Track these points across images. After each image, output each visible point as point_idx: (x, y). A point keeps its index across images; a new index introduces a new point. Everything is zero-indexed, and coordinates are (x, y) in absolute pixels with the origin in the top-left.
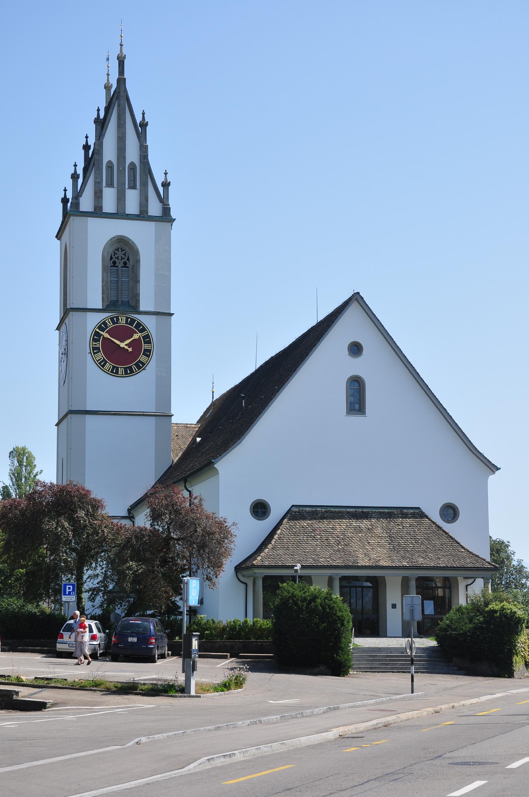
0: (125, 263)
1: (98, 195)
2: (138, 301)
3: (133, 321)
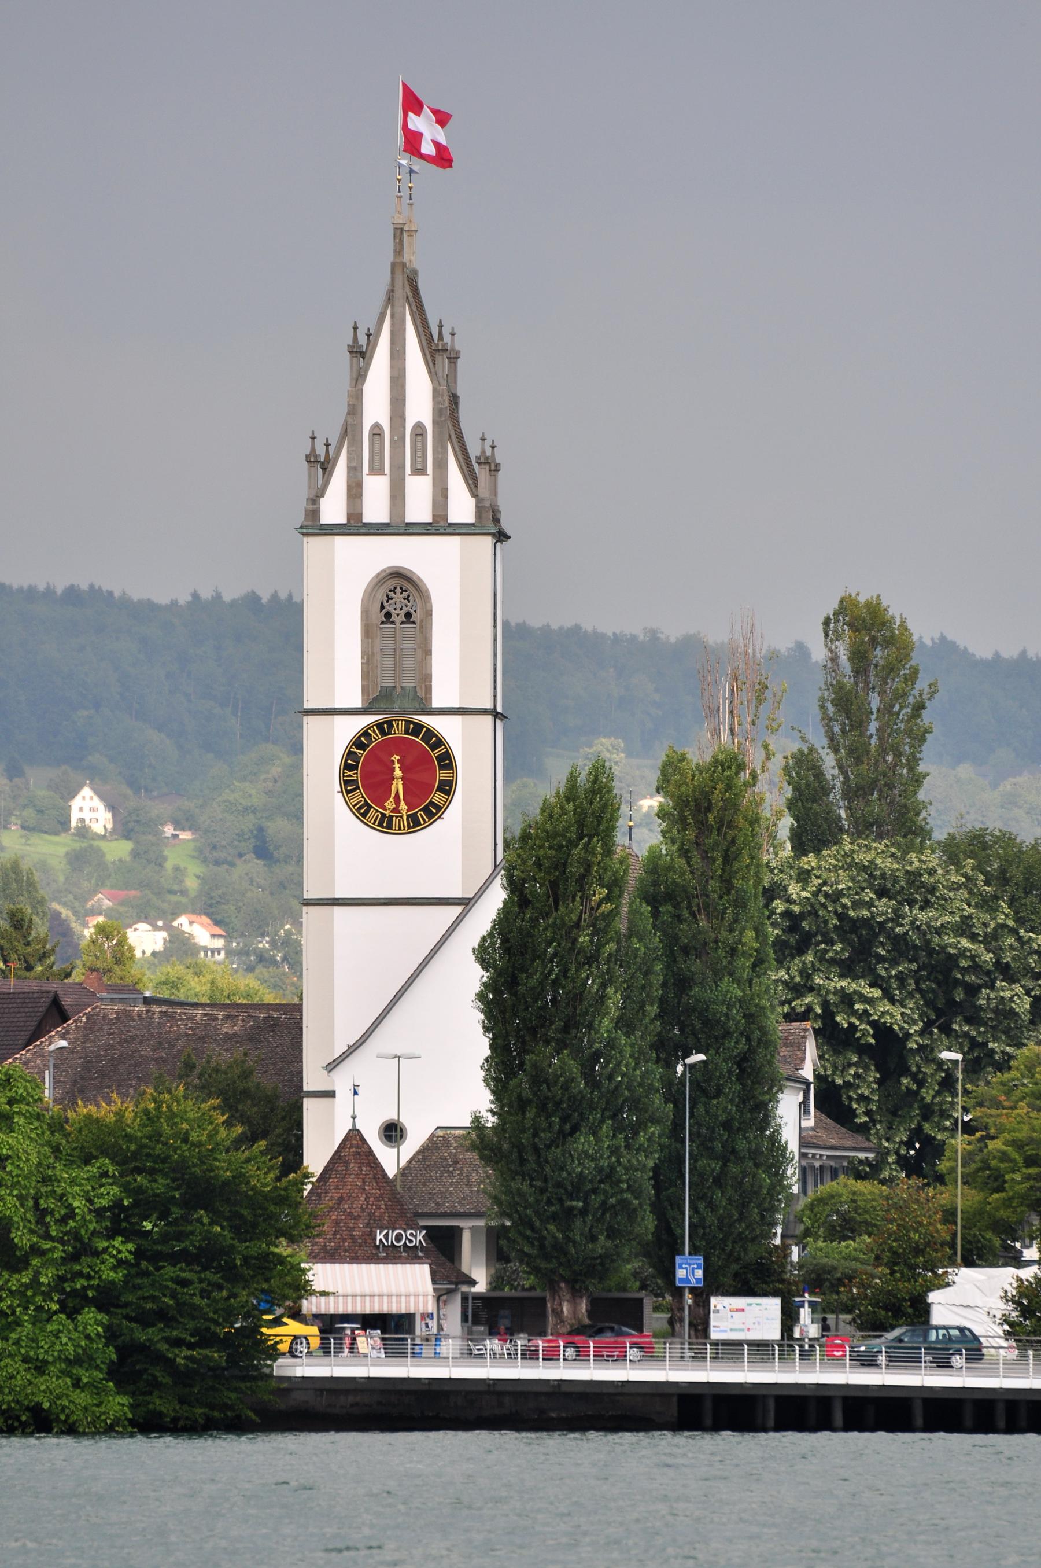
0: (408, 615)
1: (355, 492)
2: (429, 690)
3: (418, 728)
